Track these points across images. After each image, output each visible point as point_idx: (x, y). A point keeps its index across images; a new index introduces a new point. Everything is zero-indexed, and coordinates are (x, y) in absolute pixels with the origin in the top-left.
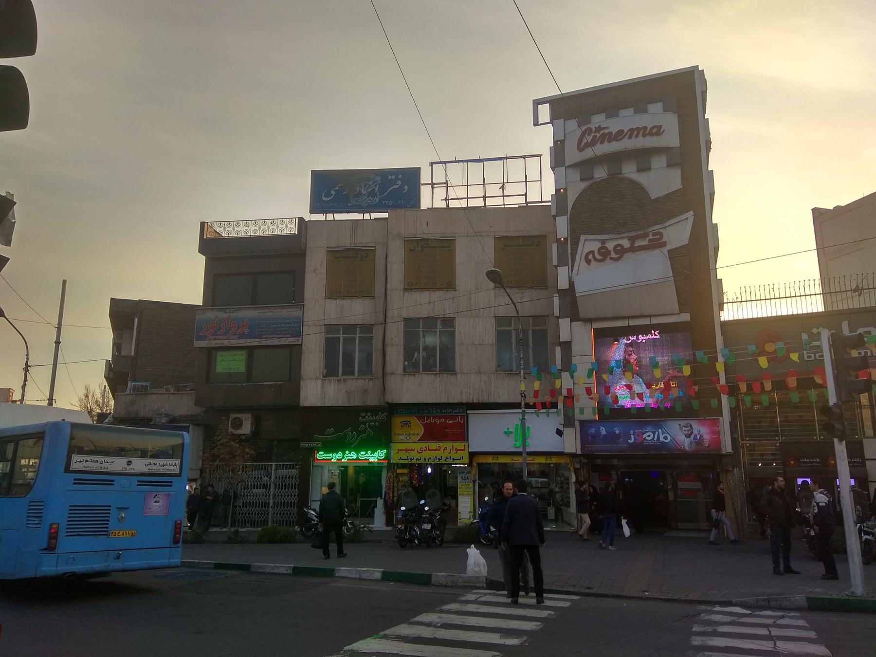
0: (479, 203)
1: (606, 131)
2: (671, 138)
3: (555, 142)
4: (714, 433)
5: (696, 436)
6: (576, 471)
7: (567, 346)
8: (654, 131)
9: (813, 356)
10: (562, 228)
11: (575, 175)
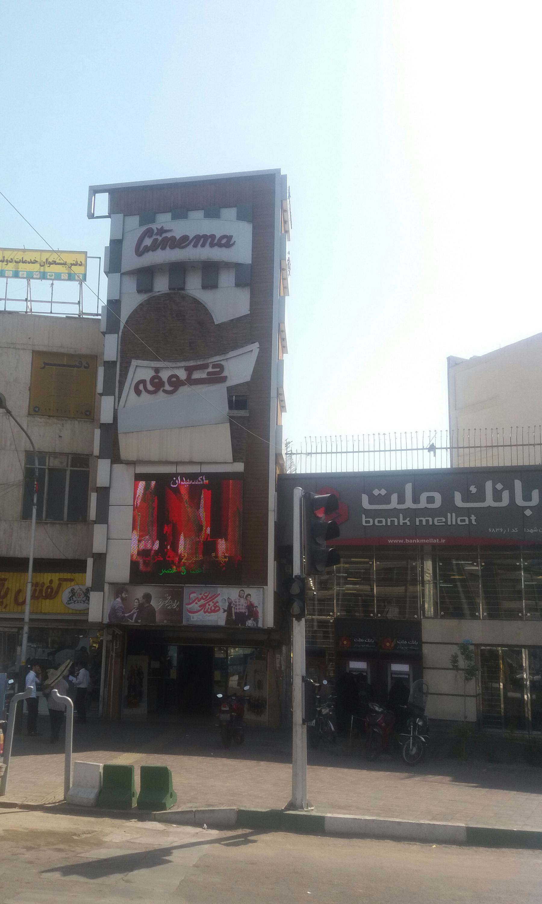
0: (20, 307)
1: (169, 235)
2: (242, 252)
3: (112, 242)
7: (104, 493)
8: (224, 241)
9: (371, 520)
10: (111, 348)
11: (131, 285)
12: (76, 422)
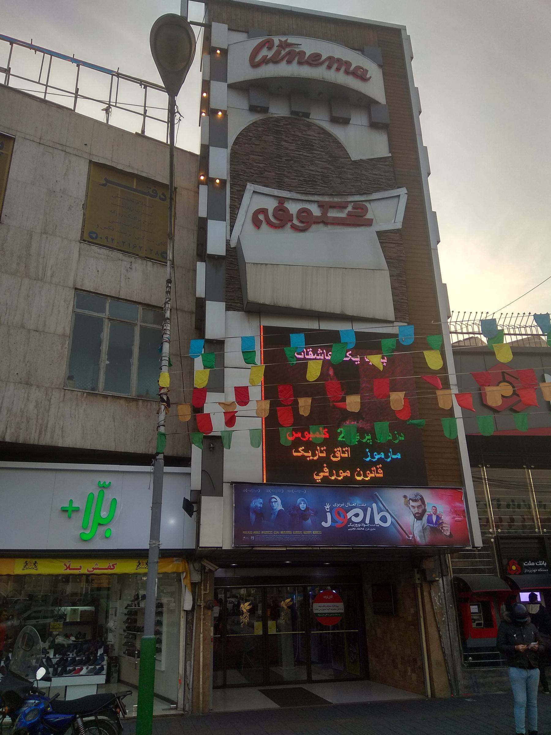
4: (456, 512)
5: (430, 516)
6: (194, 586)
12: (150, 264)
